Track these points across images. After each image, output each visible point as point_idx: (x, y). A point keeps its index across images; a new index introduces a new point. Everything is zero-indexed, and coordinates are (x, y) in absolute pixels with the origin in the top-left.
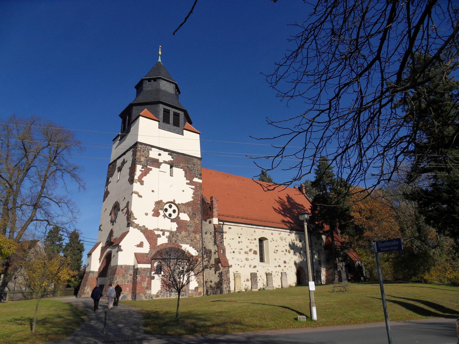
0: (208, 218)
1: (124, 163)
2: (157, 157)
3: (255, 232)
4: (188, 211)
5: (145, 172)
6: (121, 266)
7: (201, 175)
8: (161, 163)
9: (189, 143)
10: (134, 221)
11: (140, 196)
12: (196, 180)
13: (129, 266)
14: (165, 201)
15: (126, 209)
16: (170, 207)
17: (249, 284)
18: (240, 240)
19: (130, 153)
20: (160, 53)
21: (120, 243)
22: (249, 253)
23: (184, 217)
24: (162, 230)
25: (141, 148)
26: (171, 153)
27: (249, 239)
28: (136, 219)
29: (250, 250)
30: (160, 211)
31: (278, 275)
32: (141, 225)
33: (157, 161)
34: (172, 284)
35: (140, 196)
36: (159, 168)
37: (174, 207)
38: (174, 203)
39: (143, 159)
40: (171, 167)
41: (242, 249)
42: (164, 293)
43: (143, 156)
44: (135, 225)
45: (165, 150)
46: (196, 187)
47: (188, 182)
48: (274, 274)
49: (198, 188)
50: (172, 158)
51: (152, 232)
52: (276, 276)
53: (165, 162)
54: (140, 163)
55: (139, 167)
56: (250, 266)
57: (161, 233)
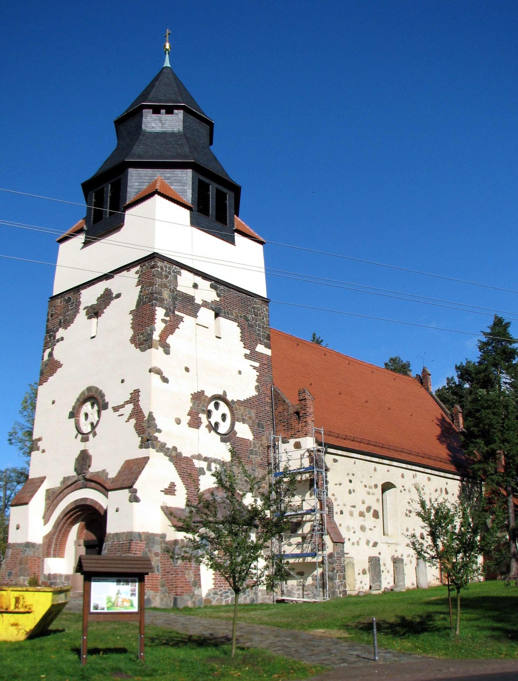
0: (292, 437)
1: (107, 298)
2: (191, 292)
3: (375, 470)
4: (250, 418)
5: (172, 327)
6: (110, 534)
7: (268, 338)
8: (198, 307)
9: (243, 262)
10: (156, 434)
11: (165, 380)
12: (261, 349)
13: (154, 535)
14: (209, 394)
15: (130, 407)
16: (217, 406)
17: (366, 580)
18: (351, 486)
19: (132, 275)
20: (168, 47)
21: (134, 483)
22: (366, 514)
23: (244, 431)
24: (206, 459)
25: (162, 268)
26: (217, 283)
27: (366, 486)
28: (159, 431)
29: (369, 509)
30: (201, 415)
31: (411, 562)
32: (169, 446)
33: (191, 299)
34: (235, 576)
35: (165, 380)
36: (196, 316)
37: (224, 408)
38: (222, 398)
39: (166, 294)
40: (217, 315)
41: (354, 507)
42: (221, 595)
43: (165, 286)
44: (159, 444)
45: (205, 277)
46: (262, 365)
47: (248, 352)
48: (405, 558)
49: (266, 368)
50: (218, 295)
51: (188, 461)
52: (409, 565)
53: (205, 304)
54: (161, 303)
55: (160, 313)
56: (368, 543)
57: (203, 465)
